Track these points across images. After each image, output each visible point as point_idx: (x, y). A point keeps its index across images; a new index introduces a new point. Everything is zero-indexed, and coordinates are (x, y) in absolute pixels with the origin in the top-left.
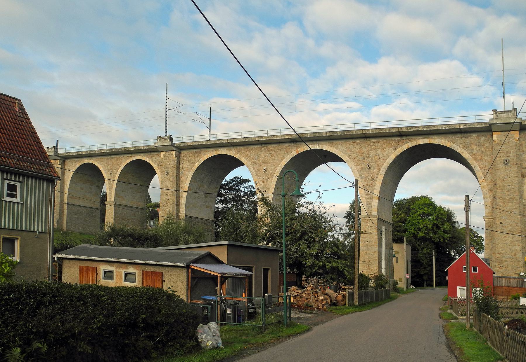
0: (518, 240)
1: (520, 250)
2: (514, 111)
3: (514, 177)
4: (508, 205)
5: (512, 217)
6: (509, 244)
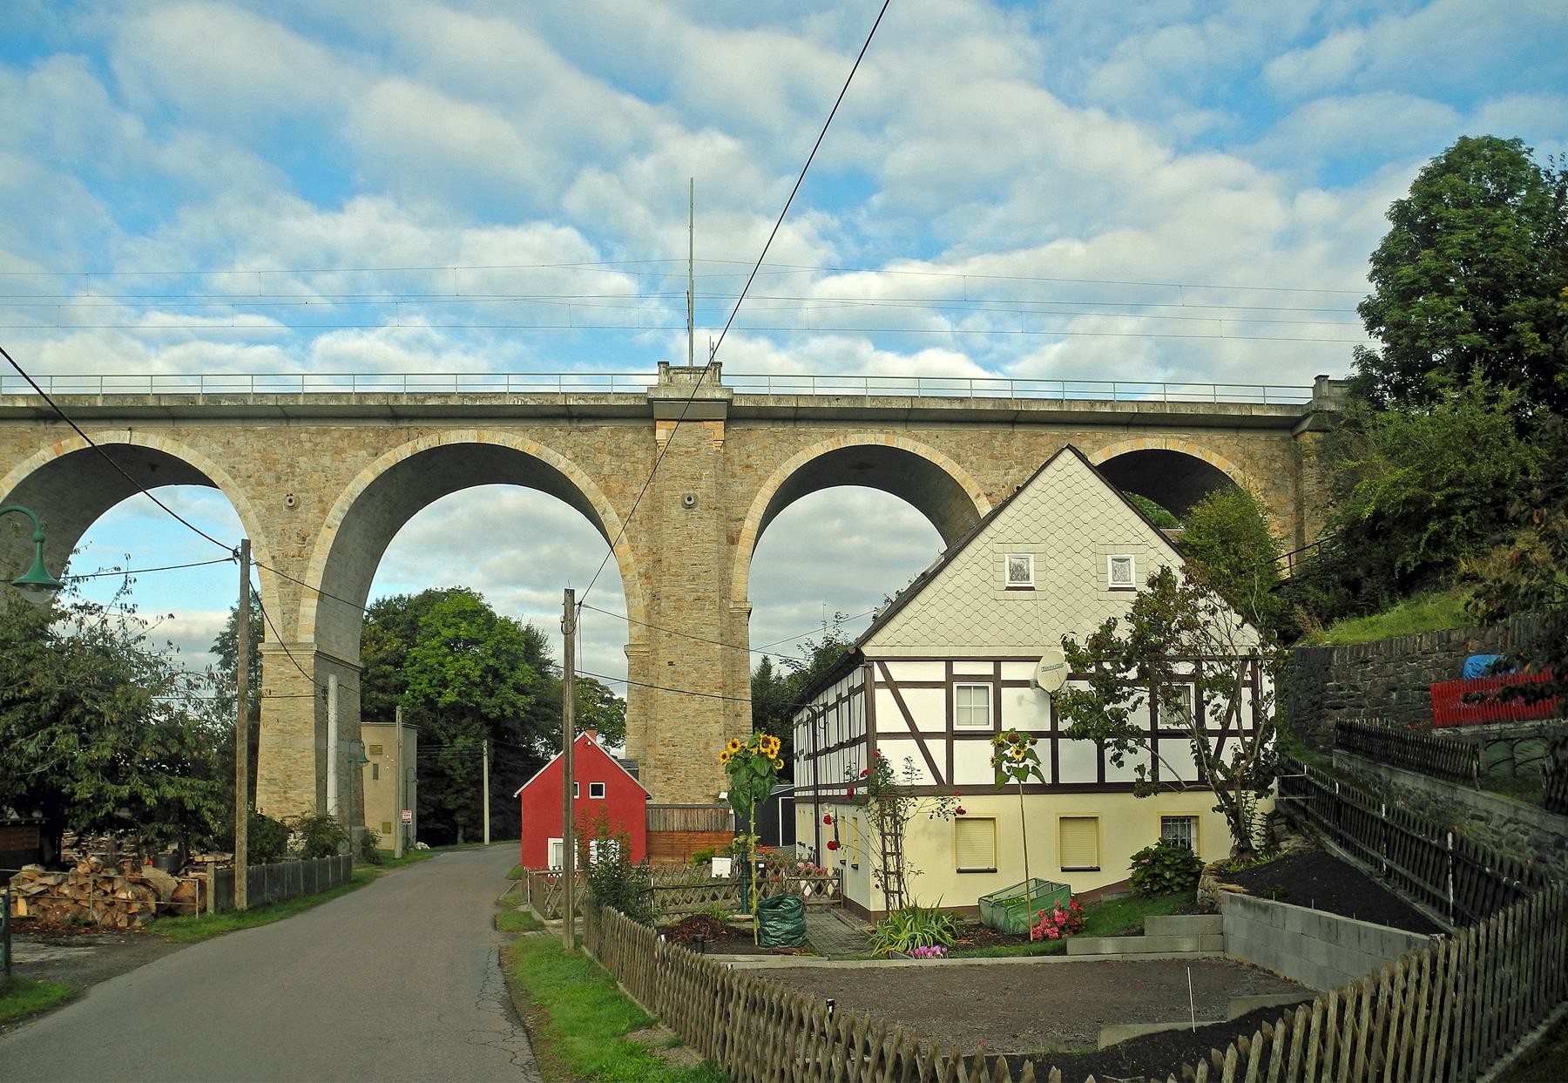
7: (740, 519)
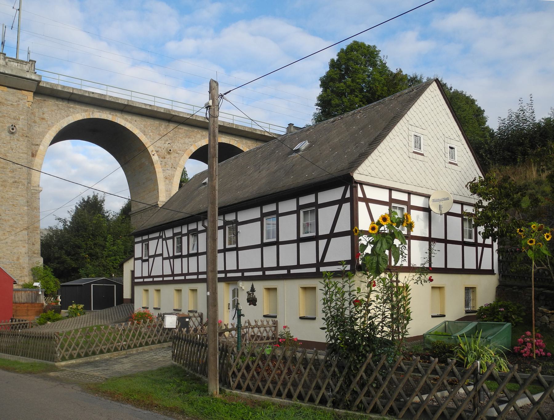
0: (22, 239)
1: (26, 253)
2: (32, 64)
3: (22, 153)
4: (11, 189)
5: (16, 208)
6: (9, 244)
7: (37, 145)
